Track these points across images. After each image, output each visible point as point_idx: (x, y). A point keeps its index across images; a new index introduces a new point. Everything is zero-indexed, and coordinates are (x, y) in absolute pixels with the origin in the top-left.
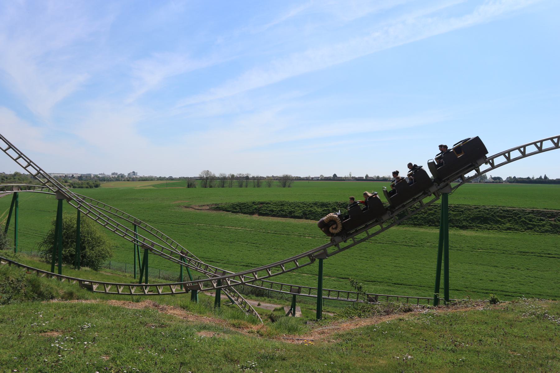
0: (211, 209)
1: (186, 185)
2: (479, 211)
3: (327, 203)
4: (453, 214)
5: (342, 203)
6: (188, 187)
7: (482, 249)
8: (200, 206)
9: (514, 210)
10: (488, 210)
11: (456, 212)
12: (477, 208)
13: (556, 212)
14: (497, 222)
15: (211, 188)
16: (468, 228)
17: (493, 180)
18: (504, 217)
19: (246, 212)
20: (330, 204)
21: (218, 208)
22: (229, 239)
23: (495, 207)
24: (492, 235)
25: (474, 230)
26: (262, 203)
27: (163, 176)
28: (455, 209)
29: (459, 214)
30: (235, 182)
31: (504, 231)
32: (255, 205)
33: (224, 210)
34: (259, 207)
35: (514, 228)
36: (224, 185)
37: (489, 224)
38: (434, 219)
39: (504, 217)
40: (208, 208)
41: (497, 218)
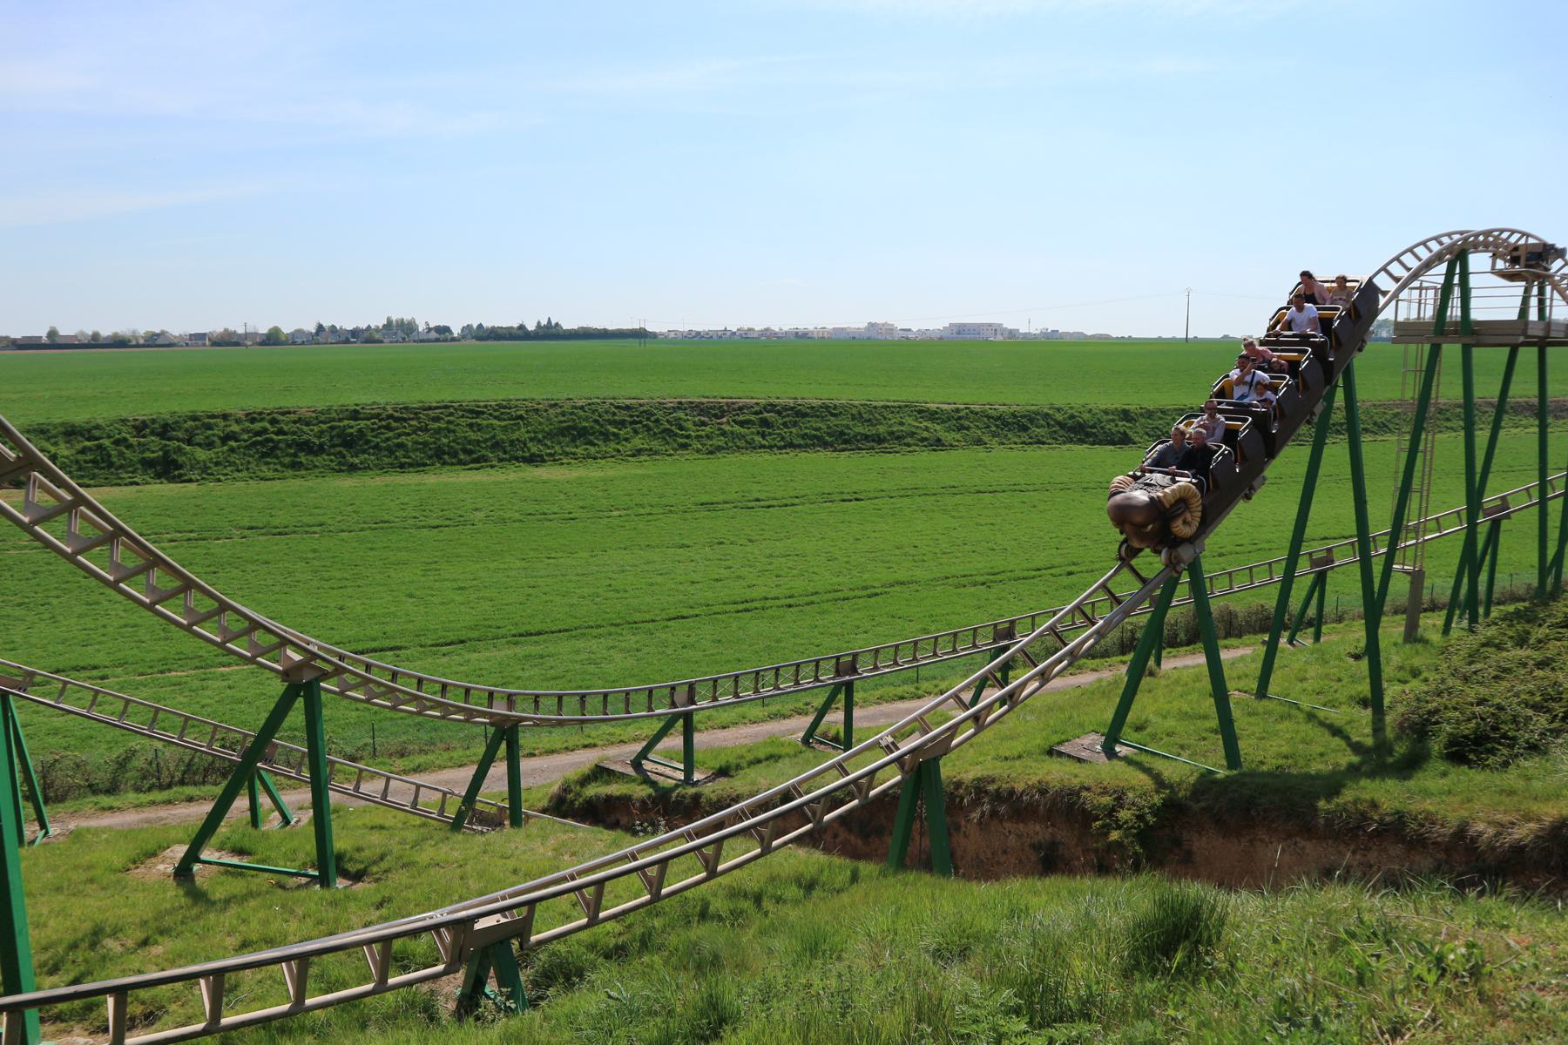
2: (563, 414)
3: (88, 426)
4: (500, 426)
5: (144, 422)
7: (618, 509)
9: (641, 405)
10: (582, 408)
11: (505, 420)
12: (556, 405)
13: (727, 404)
14: (606, 437)
16: (544, 461)
17: (437, 336)
18: (622, 423)
19: (1330, 398)
20: (97, 427)
22: (641, 526)
23: (599, 401)
24: (611, 473)
25: (562, 464)
28: (502, 413)
29: (515, 424)
31: (630, 458)
35: (651, 449)
37: (594, 445)
38: (452, 444)
39: (622, 423)
41: (609, 427)
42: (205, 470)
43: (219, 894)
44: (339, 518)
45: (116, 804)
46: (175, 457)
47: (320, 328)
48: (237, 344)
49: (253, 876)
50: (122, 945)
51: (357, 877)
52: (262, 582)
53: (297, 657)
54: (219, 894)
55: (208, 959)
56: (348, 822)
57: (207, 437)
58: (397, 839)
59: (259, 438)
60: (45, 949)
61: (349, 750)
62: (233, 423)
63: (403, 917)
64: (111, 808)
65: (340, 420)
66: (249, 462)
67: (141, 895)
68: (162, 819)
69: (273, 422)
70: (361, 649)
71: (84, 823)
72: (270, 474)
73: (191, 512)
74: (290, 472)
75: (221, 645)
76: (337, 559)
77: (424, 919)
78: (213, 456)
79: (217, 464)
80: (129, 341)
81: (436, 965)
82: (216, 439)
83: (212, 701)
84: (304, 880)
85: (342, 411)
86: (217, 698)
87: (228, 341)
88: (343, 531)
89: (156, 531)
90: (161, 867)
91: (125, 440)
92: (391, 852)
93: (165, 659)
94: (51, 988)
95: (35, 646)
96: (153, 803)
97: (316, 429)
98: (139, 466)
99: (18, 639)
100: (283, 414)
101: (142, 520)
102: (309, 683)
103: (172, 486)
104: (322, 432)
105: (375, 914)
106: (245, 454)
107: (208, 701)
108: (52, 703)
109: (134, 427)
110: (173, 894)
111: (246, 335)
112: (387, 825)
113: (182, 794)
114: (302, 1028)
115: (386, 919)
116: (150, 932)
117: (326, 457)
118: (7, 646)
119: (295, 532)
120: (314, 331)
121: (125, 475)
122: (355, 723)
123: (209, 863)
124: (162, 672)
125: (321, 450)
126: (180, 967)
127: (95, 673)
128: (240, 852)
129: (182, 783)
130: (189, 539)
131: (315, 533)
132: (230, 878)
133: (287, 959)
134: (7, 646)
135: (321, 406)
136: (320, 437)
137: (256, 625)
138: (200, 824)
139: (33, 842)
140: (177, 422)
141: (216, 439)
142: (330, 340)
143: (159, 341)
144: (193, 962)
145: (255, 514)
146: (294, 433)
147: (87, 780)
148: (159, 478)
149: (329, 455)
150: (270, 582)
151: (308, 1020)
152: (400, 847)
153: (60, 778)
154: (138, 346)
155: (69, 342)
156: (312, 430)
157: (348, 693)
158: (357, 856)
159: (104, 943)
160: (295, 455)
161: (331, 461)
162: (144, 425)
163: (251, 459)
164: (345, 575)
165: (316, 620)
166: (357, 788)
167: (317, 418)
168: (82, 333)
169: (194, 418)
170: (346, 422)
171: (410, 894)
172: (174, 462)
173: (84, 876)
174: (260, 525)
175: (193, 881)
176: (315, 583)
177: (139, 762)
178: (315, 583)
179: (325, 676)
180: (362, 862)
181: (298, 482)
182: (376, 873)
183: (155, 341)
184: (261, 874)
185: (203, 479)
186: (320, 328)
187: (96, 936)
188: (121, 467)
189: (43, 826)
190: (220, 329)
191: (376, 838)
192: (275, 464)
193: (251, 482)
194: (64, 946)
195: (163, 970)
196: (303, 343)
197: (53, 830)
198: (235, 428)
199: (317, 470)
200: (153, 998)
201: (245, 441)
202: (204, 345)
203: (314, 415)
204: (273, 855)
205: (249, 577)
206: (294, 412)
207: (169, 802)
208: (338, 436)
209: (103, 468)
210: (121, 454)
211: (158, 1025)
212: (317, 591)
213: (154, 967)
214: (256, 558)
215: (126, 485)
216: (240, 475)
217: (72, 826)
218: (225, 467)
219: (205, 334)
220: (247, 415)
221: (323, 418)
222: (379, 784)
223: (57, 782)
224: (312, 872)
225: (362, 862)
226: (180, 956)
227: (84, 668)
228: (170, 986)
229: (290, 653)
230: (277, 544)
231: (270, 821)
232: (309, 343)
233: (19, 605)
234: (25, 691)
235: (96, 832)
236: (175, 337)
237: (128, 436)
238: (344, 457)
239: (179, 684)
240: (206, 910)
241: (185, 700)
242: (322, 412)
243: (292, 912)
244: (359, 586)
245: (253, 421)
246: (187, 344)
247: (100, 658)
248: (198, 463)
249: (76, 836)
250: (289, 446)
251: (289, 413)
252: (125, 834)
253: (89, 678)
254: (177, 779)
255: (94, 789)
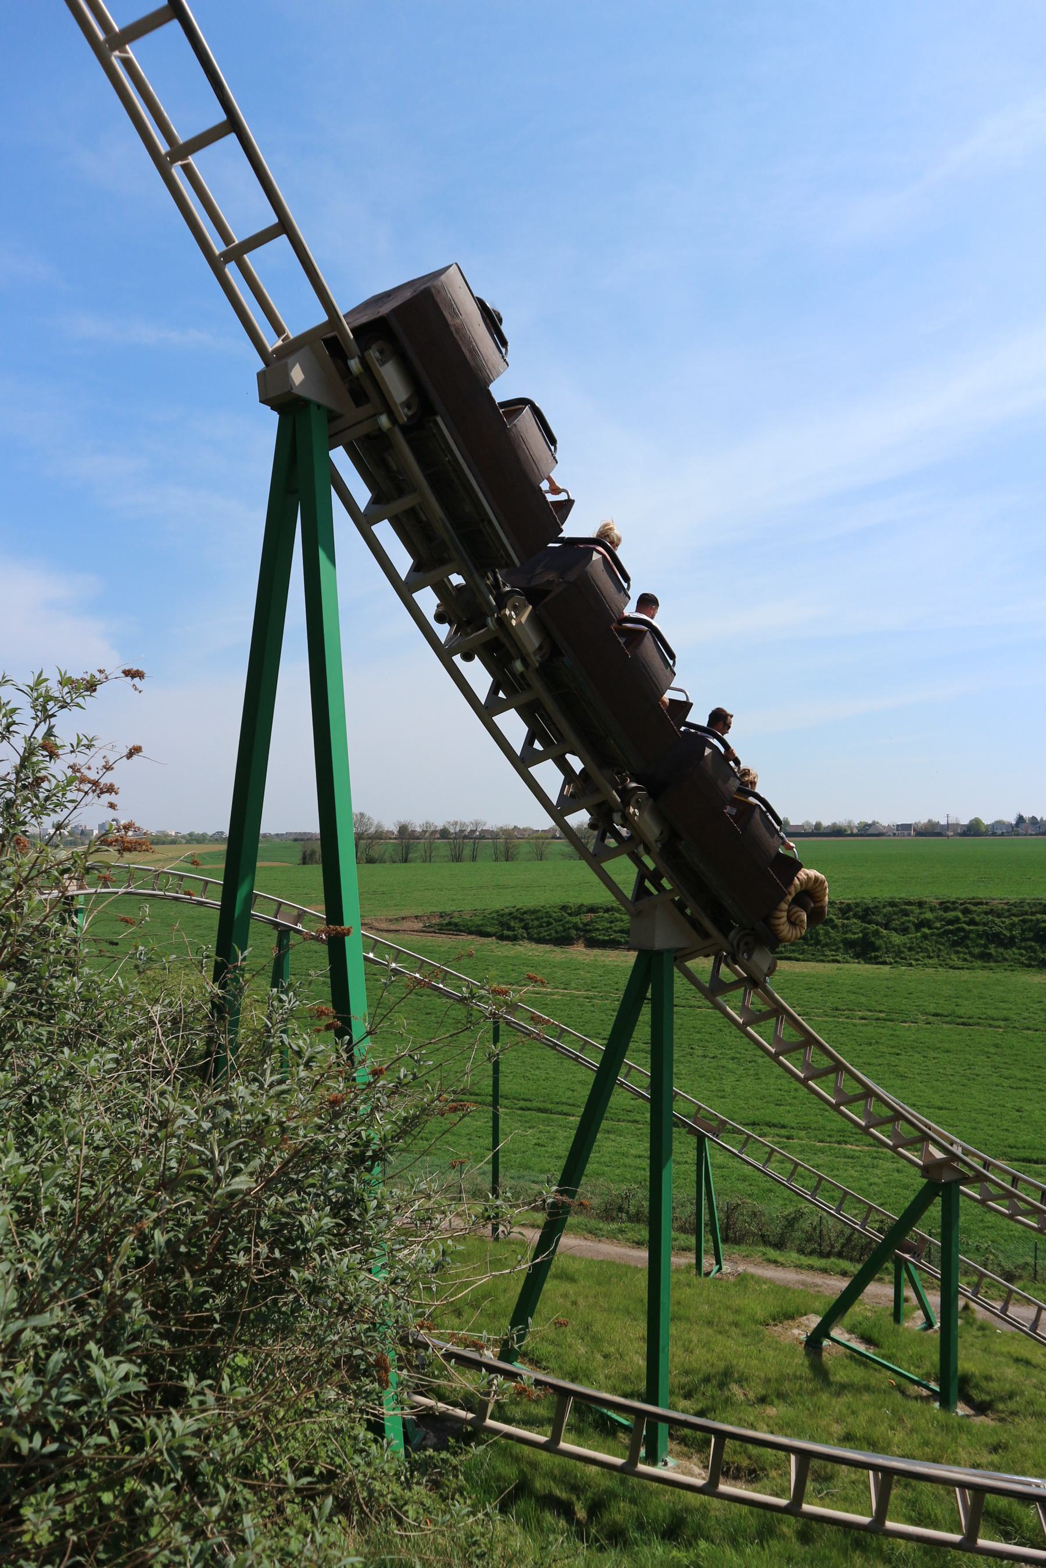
0: (427, 930)
1: (299, 856)
5: (848, 905)
6: (304, 863)
8: (391, 920)
15: (370, 865)
21: (450, 926)
26: (592, 910)
27: (198, 831)
30: (443, 847)
32: (570, 915)
33: (471, 933)
34: (585, 921)
36: (410, 856)
40: (419, 925)
42: (898, 953)
43: (840, 1376)
44: (1026, 1015)
45: (780, 1259)
46: (873, 939)
47: (1021, 819)
48: (939, 834)
49: (876, 1370)
50: (745, 1395)
51: (981, 1408)
52: (941, 1071)
53: (939, 1155)
54: (840, 1376)
55: (812, 1439)
56: (992, 1346)
57: (903, 923)
58: (1034, 1380)
59: (951, 927)
60: (687, 1373)
61: (1008, 1266)
62: (928, 910)
63: (1017, 1474)
64: (775, 1262)
65: (1033, 914)
66: (939, 950)
67: (771, 1353)
68: (817, 1285)
69: (966, 911)
70: (1035, 1158)
71: (752, 1270)
72: (960, 963)
73: (882, 993)
74: (979, 963)
75: (865, 1130)
76: (1019, 1058)
77: (1029, 1484)
78: (907, 941)
79: (910, 949)
80: (845, 830)
81: (781, 1497)
82: (910, 925)
83: (880, 1181)
84: (925, 1392)
85: (1035, 905)
86: (884, 1179)
87: (931, 831)
88: (1029, 1029)
89: (850, 1007)
90: (796, 1331)
91: (831, 920)
92: (1022, 1393)
93: (843, 1131)
94: (683, 1412)
95: (739, 1097)
96: (811, 1268)
97: (1007, 921)
98: (841, 945)
99: (728, 1089)
100: (976, 904)
101: (840, 996)
102: (948, 1184)
103: (868, 966)
104: (1013, 925)
105: (986, 1458)
106: (937, 942)
107: (876, 1180)
108: (736, 1152)
109: (840, 909)
110: (800, 1361)
111: (948, 826)
112: (1034, 1362)
113: (838, 1266)
114: (880, 1550)
115: (998, 1469)
116: (770, 1392)
117: (1016, 951)
118: (719, 1094)
119: (979, 1024)
120: (1014, 822)
121: (829, 953)
122: (1020, 1238)
123: (838, 1342)
124: (839, 1143)
125: (1009, 943)
126: (786, 1436)
127: (783, 1132)
128: (868, 1340)
129: (840, 1255)
130: (878, 1019)
131: (999, 1027)
132: (853, 1364)
133: (963, 1485)
134: (719, 1094)
135: (1014, 898)
136: (1011, 930)
137: (898, 1116)
138: (836, 1297)
139: (708, 1274)
140: (876, 907)
141: (910, 925)
142: (1030, 832)
143: (870, 831)
144: (799, 1435)
145: (941, 1001)
146: (985, 924)
147: (761, 1230)
148: (857, 958)
149: (1019, 948)
150: (949, 1071)
151: (886, 1544)
152: (1033, 1390)
153: (742, 1221)
154: (852, 835)
155: (798, 831)
156: (1003, 922)
157: (990, 1203)
158: (984, 1384)
159: (731, 1386)
160: (985, 946)
161: (1022, 955)
162: (849, 908)
163: (942, 947)
164: (1027, 1076)
165: (991, 1118)
166: (1004, 1310)
167: (1009, 910)
168: (808, 823)
169: (892, 904)
170: (1039, 916)
171: (1029, 1449)
172: (872, 944)
173: (731, 1317)
174: (945, 1013)
175: (821, 1355)
176: (994, 1079)
177: (805, 1225)
178: (994, 1079)
179: (966, 1180)
180: (988, 1393)
181: (986, 973)
182: (1003, 1412)
183: (867, 831)
184: (884, 1370)
185: (896, 962)
186: (1021, 819)
187: (725, 1377)
188: (826, 945)
189: (718, 1262)
190: (924, 820)
191: (1011, 1372)
192: (965, 953)
193: (940, 969)
194: (700, 1376)
195: (772, 1433)
196: (1002, 834)
197: (726, 1268)
198: (929, 915)
199: (1006, 964)
200: (759, 1456)
201: (938, 929)
202: (909, 835)
203: (1006, 907)
204: (899, 1355)
205: (929, 1063)
206: (987, 904)
207: (825, 1271)
208: (1030, 929)
209: (811, 945)
210: (827, 933)
211: (758, 1485)
212: (994, 1088)
213: (765, 1427)
214: (939, 1045)
215: (829, 962)
216: (931, 961)
217: (741, 1269)
218: (918, 953)
219: (910, 825)
220: (941, 904)
221: (1015, 910)
222: (1031, 1312)
223: (739, 1225)
224: (934, 1386)
225: (988, 1393)
226: (788, 1425)
227: (775, 1126)
228: (774, 1452)
229: (932, 1149)
230: (960, 1034)
231: (913, 1318)
232: (1009, 834)
233: (733, 1059)
234: (717, 1137)
235: (760, 1280)
236: (884, 827)
237: (834, 917)
238: (1035, 951)
239: (852, 1157)
240: (822, 1389)
241: (855, 1174)
242: (1014, 905)
243: (901, 1420)
244: (1040, 1090)
245: (946, 910)
246: (894, 834)
247: (789, 1119)
248: (893, 946)
249: (742, 1279)
250: (980, 936)
251: (981, 903)
252: (782, 1290)
253: (778, 1135)
254: (836, 1250)
255: (764, 1240)
